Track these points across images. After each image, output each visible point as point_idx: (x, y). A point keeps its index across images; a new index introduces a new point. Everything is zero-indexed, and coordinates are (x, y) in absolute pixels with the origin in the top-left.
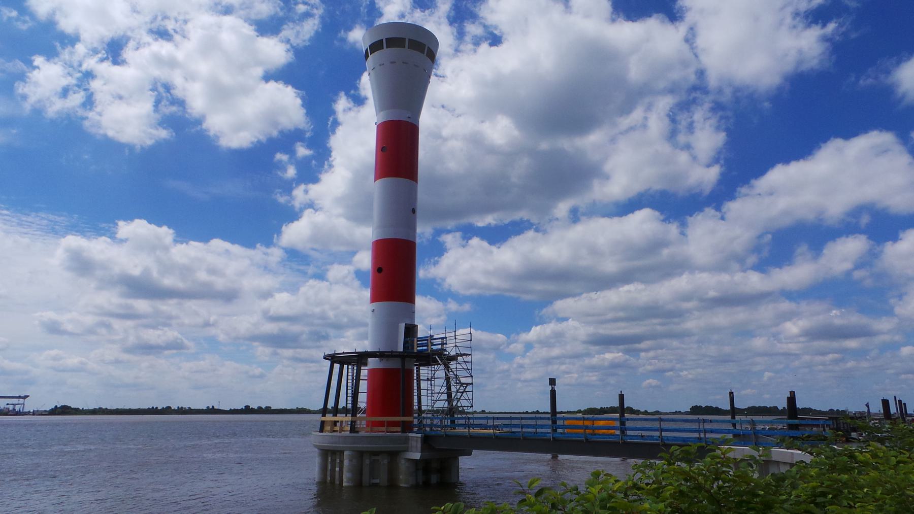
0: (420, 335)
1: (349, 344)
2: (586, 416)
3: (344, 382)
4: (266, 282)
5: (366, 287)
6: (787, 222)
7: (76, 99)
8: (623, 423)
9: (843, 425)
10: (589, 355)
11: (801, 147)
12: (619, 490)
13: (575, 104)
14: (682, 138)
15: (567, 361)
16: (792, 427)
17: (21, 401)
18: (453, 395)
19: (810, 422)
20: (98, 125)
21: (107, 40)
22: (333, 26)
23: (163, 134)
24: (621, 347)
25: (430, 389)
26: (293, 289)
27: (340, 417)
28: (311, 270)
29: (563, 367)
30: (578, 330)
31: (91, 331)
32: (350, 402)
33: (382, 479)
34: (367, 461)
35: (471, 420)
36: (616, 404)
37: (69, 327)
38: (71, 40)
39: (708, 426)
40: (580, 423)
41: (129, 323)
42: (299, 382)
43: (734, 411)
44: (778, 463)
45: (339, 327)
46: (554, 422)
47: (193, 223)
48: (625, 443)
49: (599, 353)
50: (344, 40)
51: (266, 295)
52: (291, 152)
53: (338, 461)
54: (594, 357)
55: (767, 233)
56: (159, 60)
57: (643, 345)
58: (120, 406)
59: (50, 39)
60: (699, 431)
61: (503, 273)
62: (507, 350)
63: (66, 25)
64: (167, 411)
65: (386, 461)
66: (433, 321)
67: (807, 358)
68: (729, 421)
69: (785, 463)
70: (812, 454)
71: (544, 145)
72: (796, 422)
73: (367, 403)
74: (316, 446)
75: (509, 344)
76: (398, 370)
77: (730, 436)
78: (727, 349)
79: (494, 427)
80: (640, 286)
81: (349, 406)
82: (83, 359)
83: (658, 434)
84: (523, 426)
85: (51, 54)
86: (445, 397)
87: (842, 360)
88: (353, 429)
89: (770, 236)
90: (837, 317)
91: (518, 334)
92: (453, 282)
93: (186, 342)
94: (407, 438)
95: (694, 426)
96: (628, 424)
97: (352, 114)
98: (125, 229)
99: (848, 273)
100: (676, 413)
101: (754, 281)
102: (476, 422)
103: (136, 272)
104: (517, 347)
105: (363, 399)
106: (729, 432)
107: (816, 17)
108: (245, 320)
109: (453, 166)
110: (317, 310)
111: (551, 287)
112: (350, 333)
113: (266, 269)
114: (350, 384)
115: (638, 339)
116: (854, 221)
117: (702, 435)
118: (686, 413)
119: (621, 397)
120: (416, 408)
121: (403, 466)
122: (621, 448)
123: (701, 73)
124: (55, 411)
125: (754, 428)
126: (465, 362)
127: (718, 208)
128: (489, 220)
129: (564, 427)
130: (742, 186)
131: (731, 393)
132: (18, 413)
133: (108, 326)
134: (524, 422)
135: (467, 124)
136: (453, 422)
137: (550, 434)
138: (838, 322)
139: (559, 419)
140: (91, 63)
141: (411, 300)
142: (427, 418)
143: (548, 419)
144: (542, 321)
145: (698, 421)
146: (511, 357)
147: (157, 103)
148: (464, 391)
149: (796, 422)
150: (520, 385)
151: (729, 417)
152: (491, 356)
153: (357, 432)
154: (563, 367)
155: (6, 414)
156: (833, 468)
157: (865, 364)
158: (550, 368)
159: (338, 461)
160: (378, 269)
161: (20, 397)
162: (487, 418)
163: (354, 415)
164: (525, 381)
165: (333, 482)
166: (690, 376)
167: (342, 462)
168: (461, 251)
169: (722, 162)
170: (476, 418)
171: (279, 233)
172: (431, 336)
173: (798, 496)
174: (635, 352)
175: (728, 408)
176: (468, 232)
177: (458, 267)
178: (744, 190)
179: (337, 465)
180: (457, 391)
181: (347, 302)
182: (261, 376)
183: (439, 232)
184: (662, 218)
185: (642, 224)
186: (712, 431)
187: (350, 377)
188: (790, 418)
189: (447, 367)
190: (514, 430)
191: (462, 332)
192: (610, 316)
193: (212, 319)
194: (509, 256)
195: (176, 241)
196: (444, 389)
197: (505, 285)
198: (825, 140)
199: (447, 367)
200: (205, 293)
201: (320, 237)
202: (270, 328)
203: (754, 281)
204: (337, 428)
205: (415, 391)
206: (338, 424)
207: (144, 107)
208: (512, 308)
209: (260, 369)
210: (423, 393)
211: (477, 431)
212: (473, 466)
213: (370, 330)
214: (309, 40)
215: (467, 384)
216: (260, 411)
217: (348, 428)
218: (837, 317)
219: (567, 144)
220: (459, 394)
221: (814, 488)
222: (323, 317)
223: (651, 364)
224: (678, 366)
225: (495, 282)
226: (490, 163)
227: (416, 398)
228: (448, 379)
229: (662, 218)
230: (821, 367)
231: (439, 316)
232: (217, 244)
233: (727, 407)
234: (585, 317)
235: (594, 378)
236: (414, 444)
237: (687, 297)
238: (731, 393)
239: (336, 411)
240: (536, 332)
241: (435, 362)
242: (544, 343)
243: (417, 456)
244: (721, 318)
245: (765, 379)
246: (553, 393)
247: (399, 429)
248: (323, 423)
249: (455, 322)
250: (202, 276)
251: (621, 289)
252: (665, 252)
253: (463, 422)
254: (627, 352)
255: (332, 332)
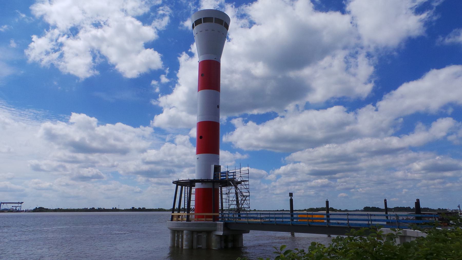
0: (222, 170)
1: (187, 175)
2: (309, 213)
3: (183, 195)
4: (143, 144)
5: (195, 147)
6: (411, 112)
7: (56, 55)
8: (328, 216)
9: (445, 217)
10: (310, 181)
11: (416, 74)
12: (326, 252)
13: (298, 54)
14: (352, 70)
15: (298, 184)
16: (417, 218)
17: (20, 205)
18: (239, 202)
19: (428, 215)
20: (66, 68)
21: (69, 27)
22: (176, 20)
23: (97, 73)
24: (326, 176)
25: (227, 199)
26: (157, 147)
27: (181, 213)
28: (168, 138)
29: (297, 187)
30: (304, 167)
31: (55, 169)
32: (186, 205)
33: (203, 245)
34: (195, 236)
35: (249, 214)
36: (325, 206)
37: (44, 167)
38: (55, 27)
39: (373, 218)
40: (306, 216)
41: (76, 165)
42: (161, 195)
43: (387, 210)
44: (410, 237)
45: (180, 167)
46: (292, 216)
47: (106, 114)
48: (329, 227)
49: (315, 179)
50: (182, 26)
51: (143, 151)
52: (159, 80)
53: (181, 236)
54: (312, 181)
55: (401, 117)
56: (95, 38)
57: (337, 175)
58: (69, 208)
59: (41, 27)
60: (368, 220)
61: (266, 139)
62: (267, 178)
63: (51, 21)
64: (93, 210)
65: (205, 236)
66: (229, 164)
67: (424, 182)
68: (384, 215)
69: (414, 237)
70: (426, 233)
71: (280, 76)
72: (420, 215)
73: (195, 206)
74: (169, 228)
75: (267, 176)
76: (211, 189)
77: (385, 223)
78: (382, 177)
79: (261, 218)
80: (335, 145)
81: (186, 207)
82: (51, 184)
83: (346, 222)
84: (276, 218)
85: (40, 34)
86: (235, 203)
87: (444, 183)
88: (188, 220)
89: (402, 119)
90: (439, 160)
91: (274, 170)
92: (240, 144)
93: (103, 175)
94: (216, 224)
95: (366, 217)
96: (331, 217)
97: (189, 62)
98: (76, 117)
99: (445, 138)
100: (356, 211)
101: (395, 142)
102: (251, 216)
103: (77, 139)
104: (272, 176)
105: (193, 204)
106: (384, 221)
107: (419, 10)
108: (133, 164)
109: (237, 86)
110: (169, 159)
111: (288, 146)
112: (186, 170)
113: (143, 137)
114: (186, 196)
115: (335, 172)
116: (444, 111)
117: (370, 223)
118: (362, 211)
119: (327, 202)
120: (220, 208)
121: (214, 238)
122: (327, 229)
123: (359, 38)
124: (36, 210)
125: (398, 219)
126: (246, 185)
127: (374, 105)
128: (255, 112)
129: (297, 218)
130: (386, 94)
131: (385, 200)
132: (18, 211)
133: (64, 167)
134: (276, 216)
135: (241, 65)
136: (239, 216)
137: (291, 222)
138: (440, 163)
139: (295, 214)
140: (62, 39)
141: (217, 152)
142: (226, 214)
143: (289, 214)
144: (285, 164)
145: (368, 215)
146: (269, 182)
147: (94, 58)
148: (245, 200)
149: (420, 215)
150: (274, 196)
151: (384, 213)
152: (259, 181)
153: (190, 221)
154: (297, 187)
155: (12, 212)
156: (437, 240)
157: (457, 185)
158: (290, 187)
159: (181, 236)
160: (200, 137)
161: (19, 203)
162: (257, 214)
163: (188, 212)
164: (277, 194)
165: (178, 247)
166: (363, 192)
167: (182, 236)
168: (243, 128)
169: (373, 82)
170: (252, 214)
171: (152, 118)
172: (228, 171)
173: (418, 255)
174: (335, 179)
175: (384, 208)
176: (247, 119)
177: (241, 136)
178: (387, 96)
179: (180, 238)
180: (242, 200)
181: (186, 154)
182: (140, 192)
183: (230, 119)
184: (345, 110)
185: (335, 113)
186: (375, 220)
187: (186, 193)
188: (416, 213)
189: (236, 188)
190: (271, 220)
191: (244, 169)
192: (320, 160)
193: (116, 163)
194: (267, 130)
195: (98, 124)
196: (235, 199)
197: (268, 145)
198: (428, 70)
199: (236, 188)
200: (113, 150)
201: (173, 121)
202: (145, 167)
203: (395, 142)
204: (180, 219)
205: (220, 200)
206: (180, 217)
207: (88, 60)
208: (270, 156)
209: (140, 189)
210: (224, 201)
211: (252, 220)
212: (249, 239)
213: (196, 168)
214: (166, 27)
215: (247, 196)
216: (140, 210)
217: (186, 219)
218: (439, 160)
219: (292, 74)
220: (243, 201)
221: (427, 251)
222: (172, 162)
223: (342, 185)
224: (357, 186)
225: (262, 144)
226: (255, 84)
227: (220, 203)
228: (236, 194)
229: (345, 110)
230: (433, 186)
231: (231, 161)
232: (120, 125)
233: (383, 207)
234: (310, 162)
235: (313, 193)
236: (219, 227)
237: (360, 150)
238: (385, 200)
239: (179, 210)
240: (283, 169)
241: (230, 185)
242: (288, 174)
243: (221, 233)
244: (378, 161)
245: (403, 193)
246: (291, 201)
247: (212, 219)
248: (172, 216)
249: (240, 164)
250: (112, 142)
251: (325, 147)
252: (347, 128)
253: (245, 216)
254: (330, 179)
255: (176, 169)
